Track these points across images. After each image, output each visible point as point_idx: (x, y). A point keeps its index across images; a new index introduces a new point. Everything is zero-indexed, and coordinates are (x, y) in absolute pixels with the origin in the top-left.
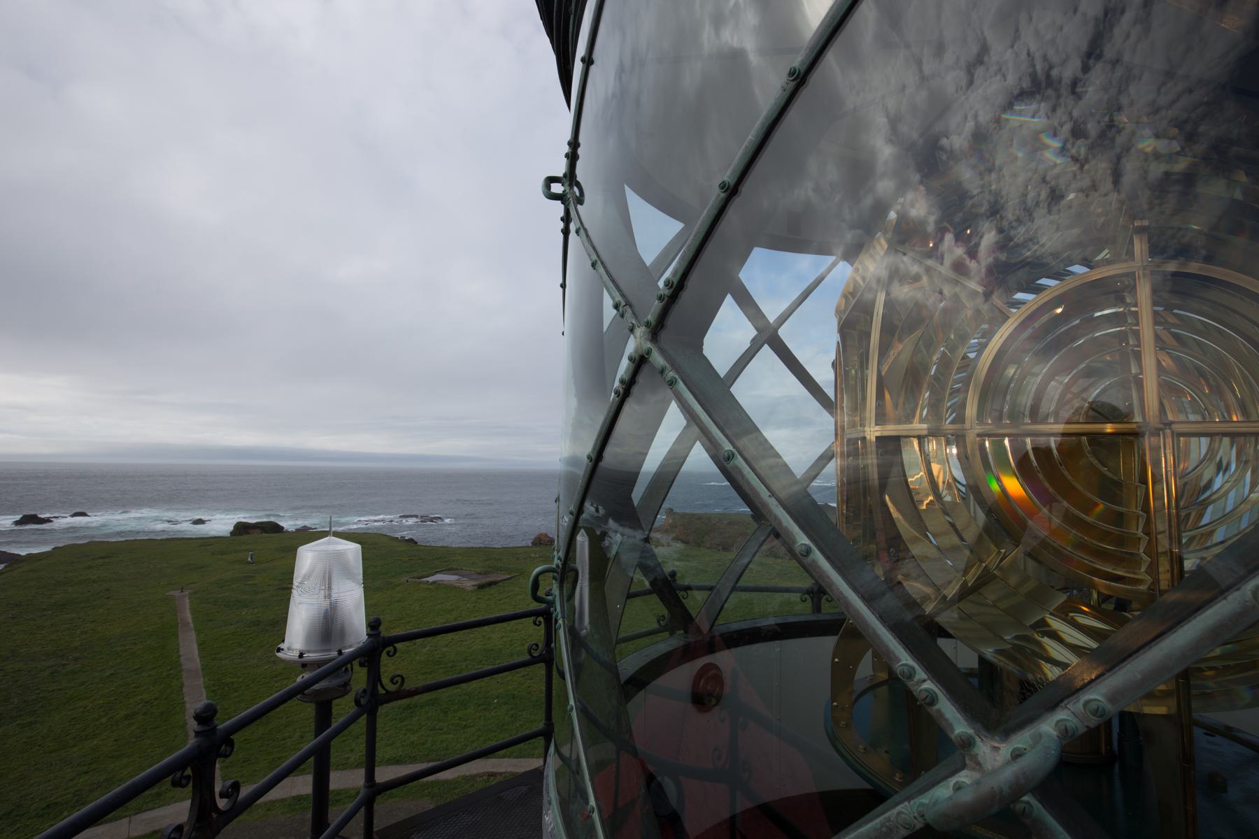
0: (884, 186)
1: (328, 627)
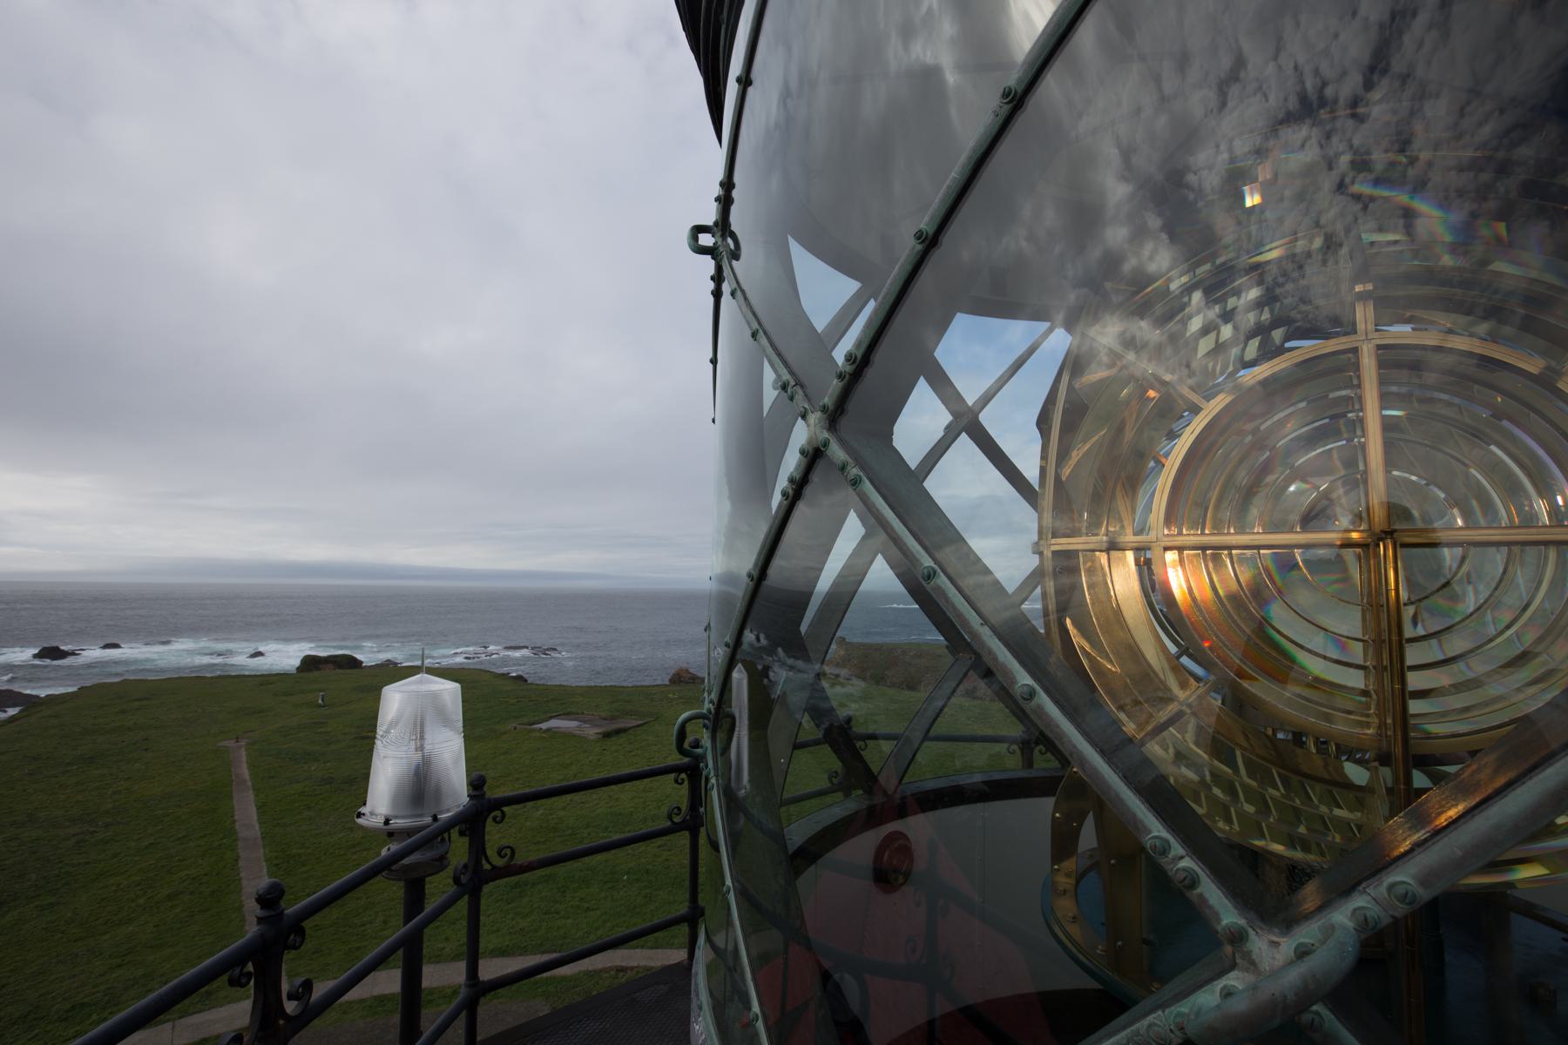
0: (1116, 235)
1: (420, 786)
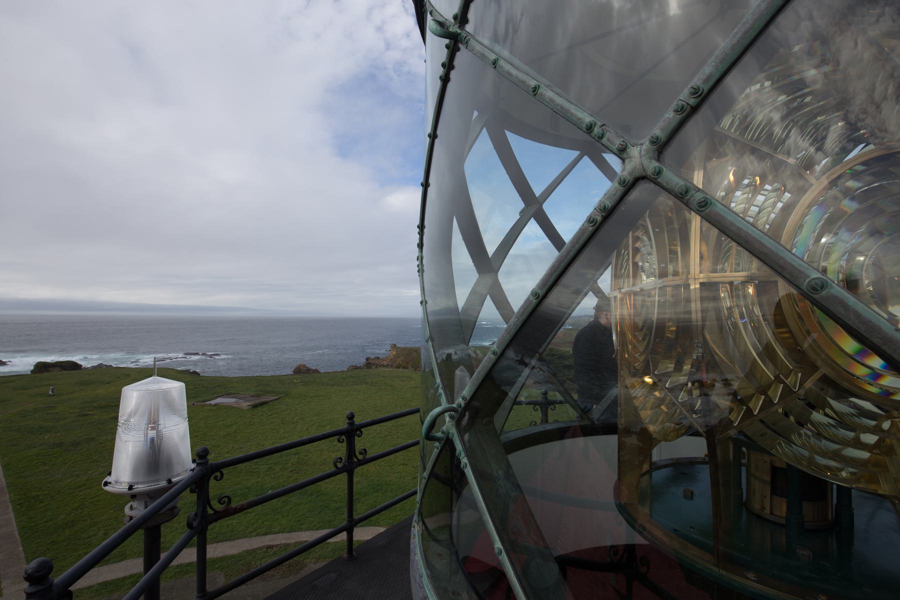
1: (155, 457)
